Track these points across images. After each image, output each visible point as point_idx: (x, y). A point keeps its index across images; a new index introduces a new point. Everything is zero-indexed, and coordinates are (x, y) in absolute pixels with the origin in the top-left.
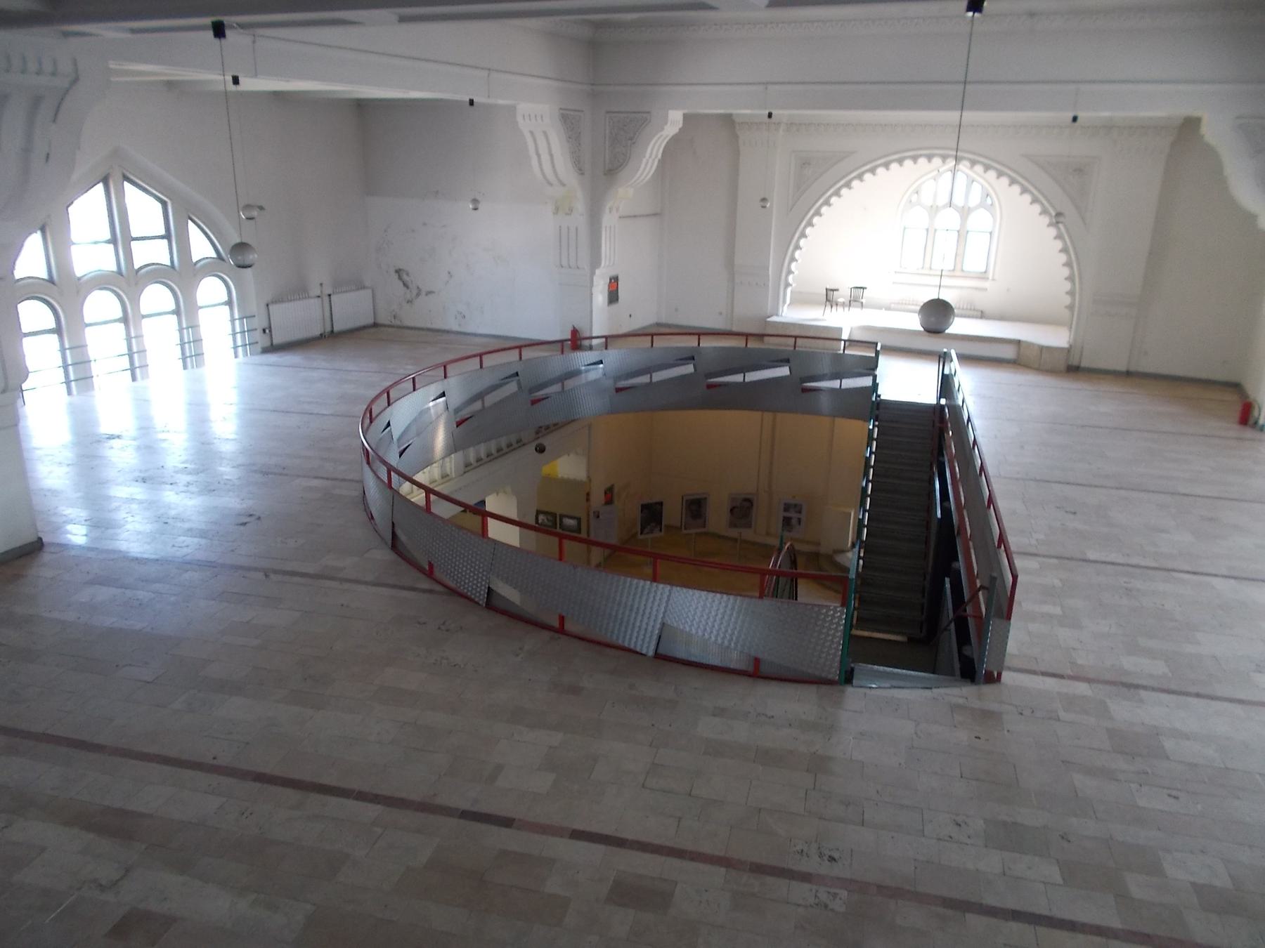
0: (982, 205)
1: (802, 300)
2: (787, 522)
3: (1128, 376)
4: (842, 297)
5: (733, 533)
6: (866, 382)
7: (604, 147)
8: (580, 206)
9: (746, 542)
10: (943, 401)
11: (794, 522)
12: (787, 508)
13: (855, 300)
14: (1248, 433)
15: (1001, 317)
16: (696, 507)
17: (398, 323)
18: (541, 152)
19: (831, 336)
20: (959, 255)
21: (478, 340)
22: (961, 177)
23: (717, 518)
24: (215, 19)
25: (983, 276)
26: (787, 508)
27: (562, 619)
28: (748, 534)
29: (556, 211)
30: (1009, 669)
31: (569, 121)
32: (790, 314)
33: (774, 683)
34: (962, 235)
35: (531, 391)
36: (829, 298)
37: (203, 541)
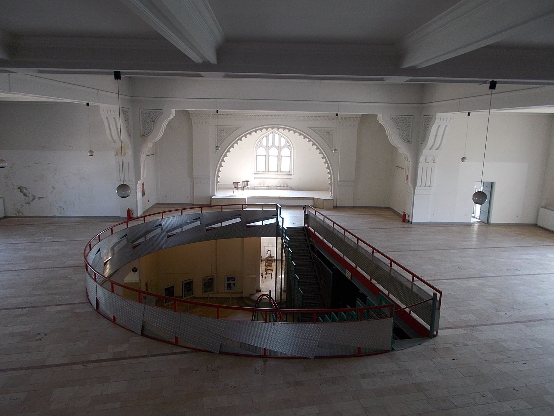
0: (285, 146)
1: (225, 188)
2: (229, 286)
3: (353, 208)
4: (240, 186)
5: (206, 295)
6: (273, 221)
7: (141, 124)
8: (130, 152)
9: (211, 298)
10: (306, 225)
11: (232, 285)
12: (228, 279)
13: (246, 185)
14: (406, 225)
15: (298, 189)
16: (188, 286)
17: (21, 215)
18: (111, 127)
19: (241, 203)
21: (73, 219)
23: (198, 290)
25: (289, 173)
26: (228, 279)
28: (211, 295)
29: (117, 154)
30: (442, 329)
31: (124, 112)
32: (220, 194)
33: (369, 357)
35: (133, 242)
36: (235, 187)
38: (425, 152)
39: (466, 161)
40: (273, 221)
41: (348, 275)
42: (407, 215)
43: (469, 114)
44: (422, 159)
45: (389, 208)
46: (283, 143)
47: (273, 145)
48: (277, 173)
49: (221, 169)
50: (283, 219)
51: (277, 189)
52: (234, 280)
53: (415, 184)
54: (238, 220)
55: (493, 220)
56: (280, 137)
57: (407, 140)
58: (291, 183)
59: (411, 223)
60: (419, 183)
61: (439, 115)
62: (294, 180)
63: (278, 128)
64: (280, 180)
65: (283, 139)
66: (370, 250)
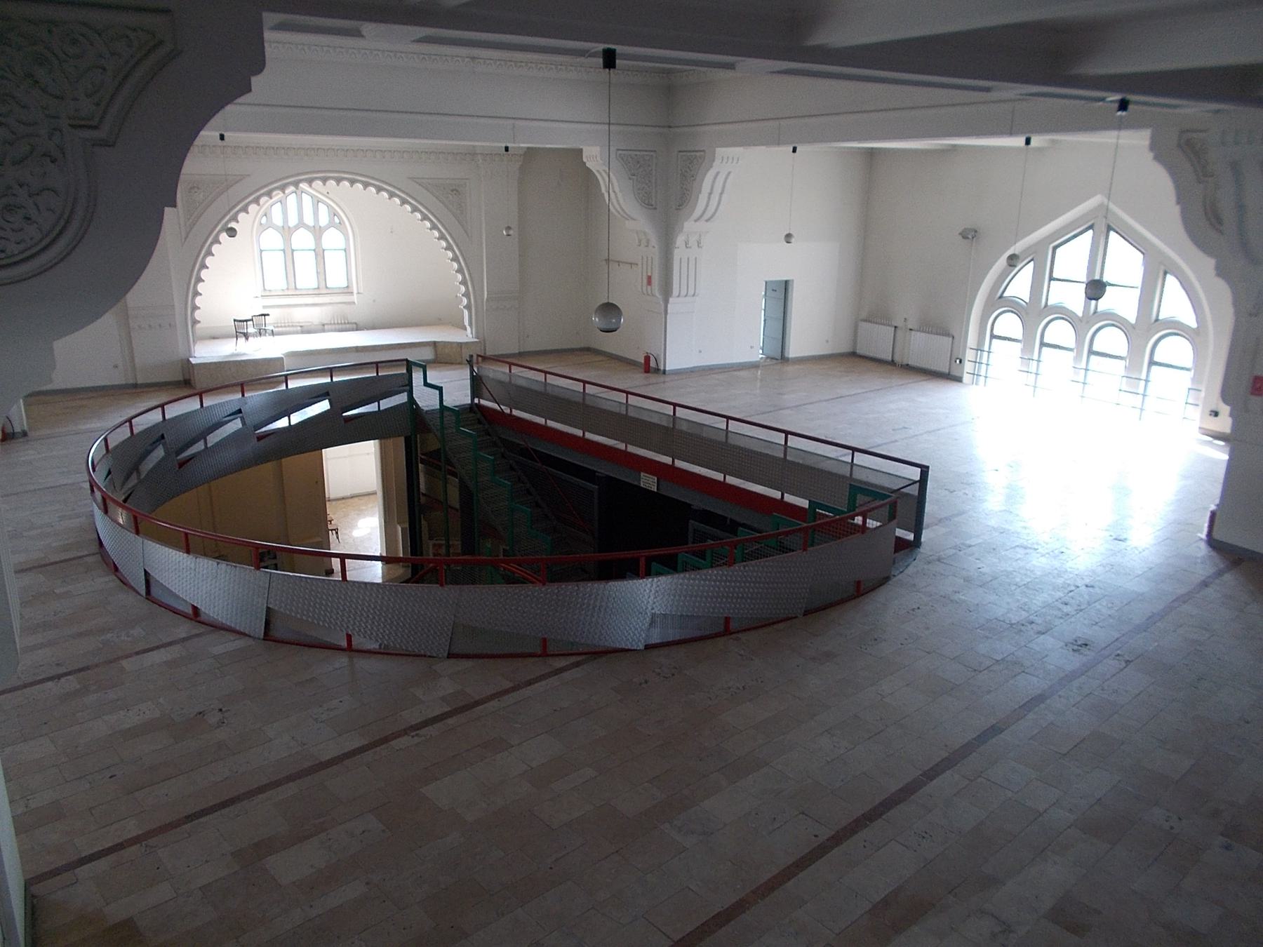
0: (331, 225)
6: (401, 398)
10: (476, 401)
20: (321, 272)
22: (307, 200)
24: (607, 46)
25: (347, 291)
27: (349, 637)
32: (204, 353)
34: (320, 254)
36: (240, 330)
37: (968, 542)
38: (689, 227)
39: (793, 240)
40: (401, 398)
41: (649, 482)
42: (652, 359)
43: (794, 150)
44: (680, 240)
45: (588, 350)
46: (324, 219)
47: (301, 224)
48: (317, 292)
49: (200, 287)
50: (440, 389)
51: (324, 331)
52: (275, 558)
53: (667, 291)
54: (324, 406)
55: (793, 351)
56: (317, 201)
57: (647, 203)
58: (355, 315)
59: (664, 372)
60: (675, 292)
61: (721, 151)
62: (361, 304)
63: (310, 182)
64: (330, 307)
65: (323, 209)
66: (721, 423)
